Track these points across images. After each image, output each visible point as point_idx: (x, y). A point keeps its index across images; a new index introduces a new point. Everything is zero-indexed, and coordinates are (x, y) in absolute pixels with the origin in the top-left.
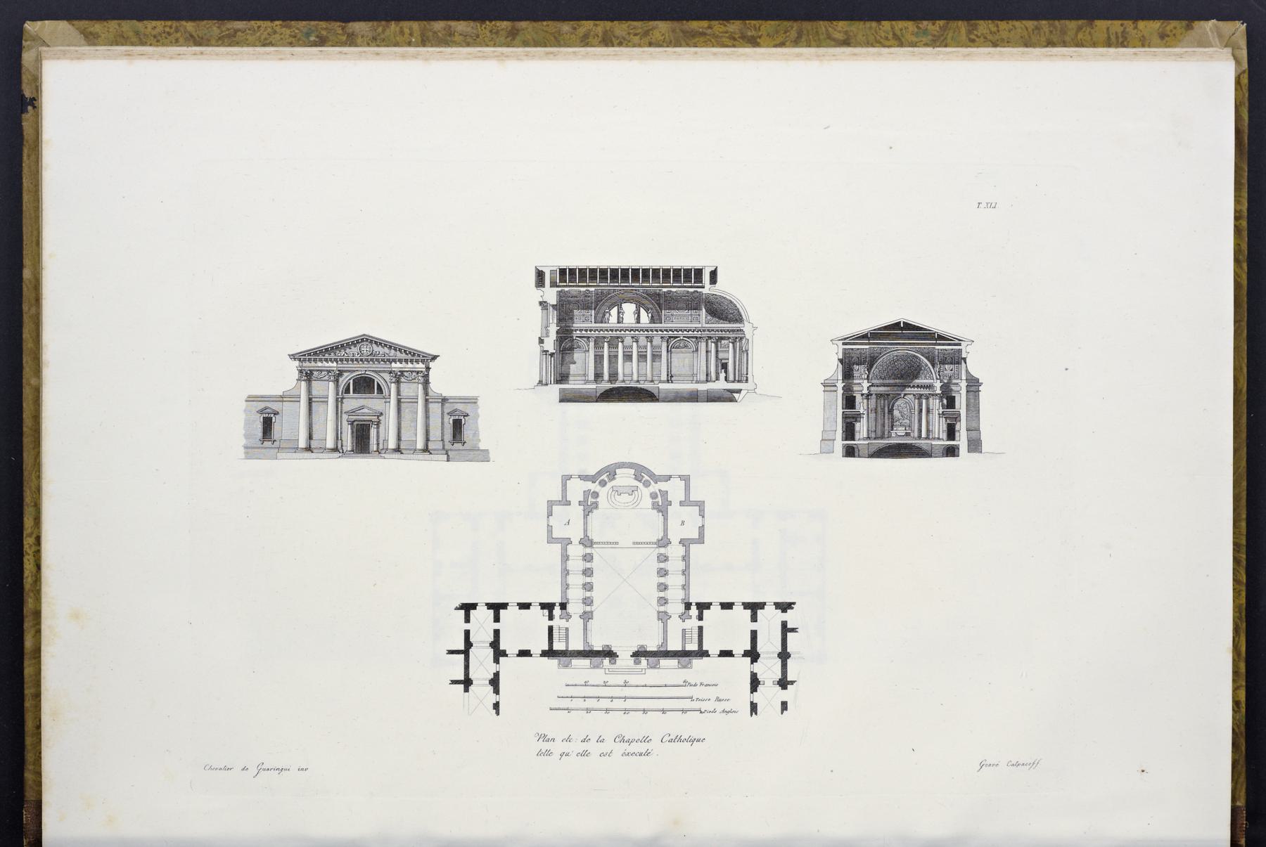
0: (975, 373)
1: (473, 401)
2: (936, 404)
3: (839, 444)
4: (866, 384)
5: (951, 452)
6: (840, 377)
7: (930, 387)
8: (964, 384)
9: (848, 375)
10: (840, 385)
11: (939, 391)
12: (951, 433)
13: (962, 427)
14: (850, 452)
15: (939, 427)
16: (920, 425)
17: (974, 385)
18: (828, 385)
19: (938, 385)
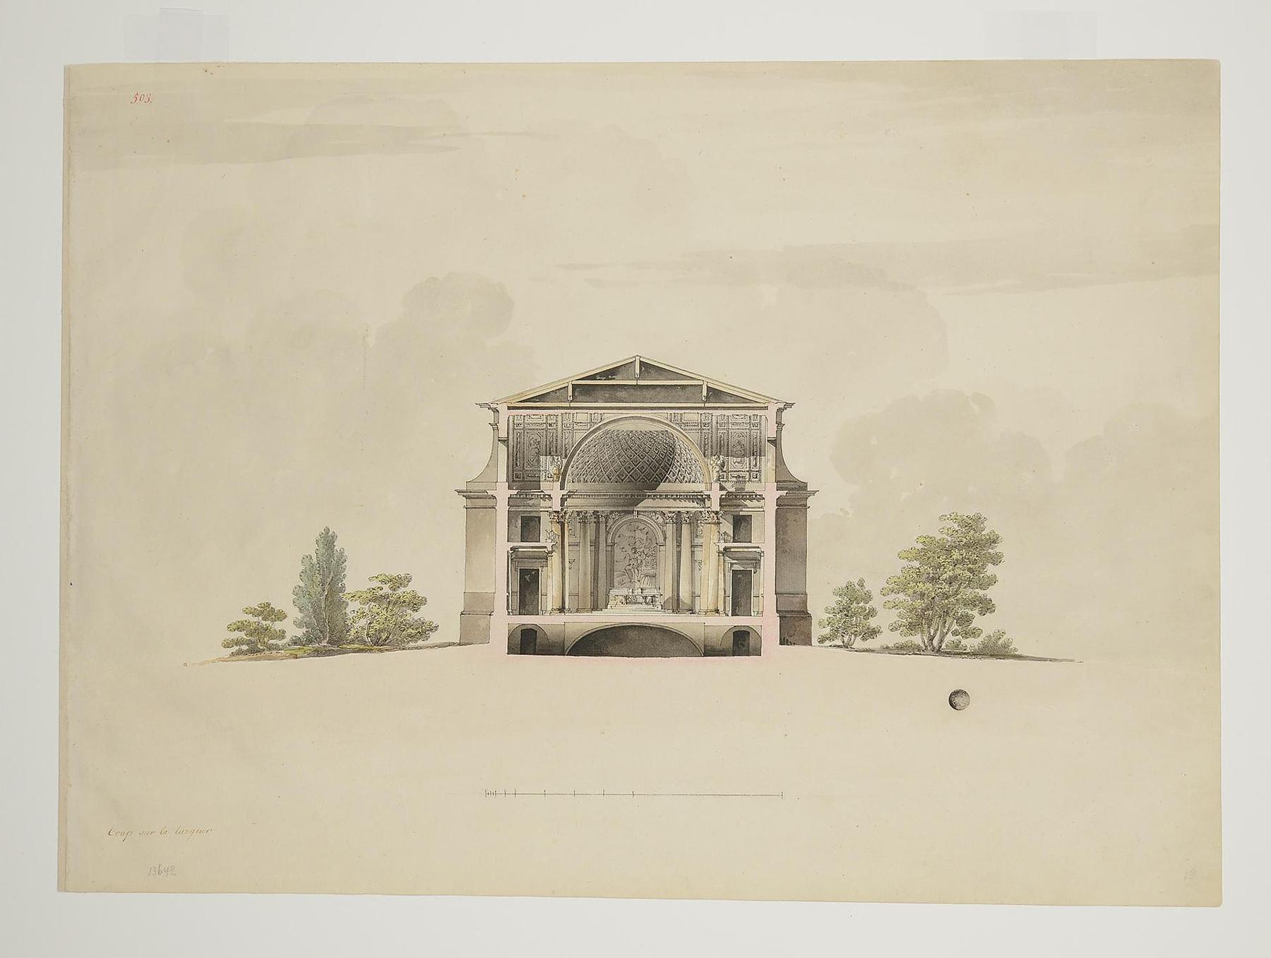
0: (798, 470)
1: (758, 652)
2: (713, 539)
3: (503, 623)
4: (557, 494)
5: (742, 643)
6: (503, 476)
7: (702, 499)
8: (771, 494)
9: (523, 479)
10: (503, 493)
11: (716, 507)
12: (740, 592)
13: (765, 582)
14: (527, 642)
15: (711, 582)
16: (537, 408)
17: (794, 499)
18: (477, 499)
19: (716, 494)
